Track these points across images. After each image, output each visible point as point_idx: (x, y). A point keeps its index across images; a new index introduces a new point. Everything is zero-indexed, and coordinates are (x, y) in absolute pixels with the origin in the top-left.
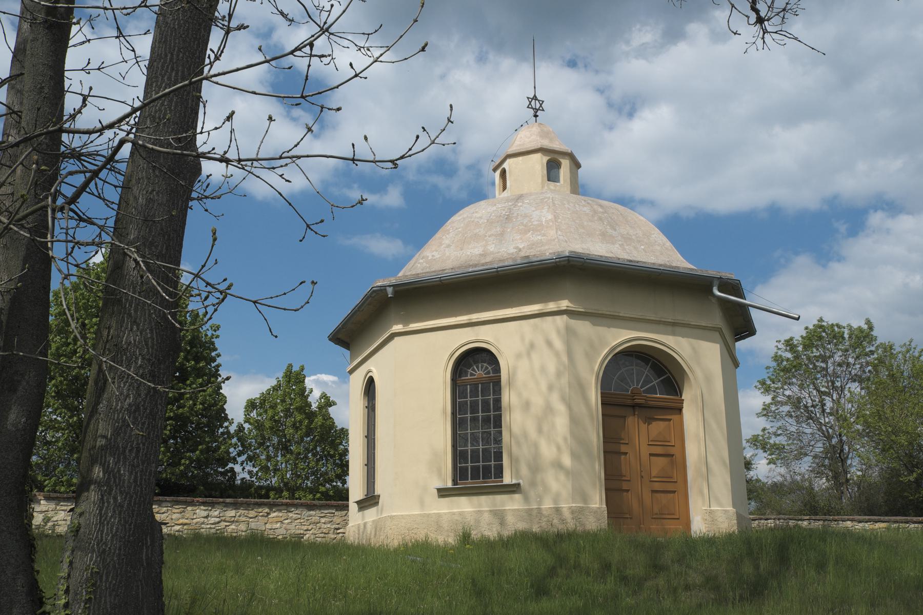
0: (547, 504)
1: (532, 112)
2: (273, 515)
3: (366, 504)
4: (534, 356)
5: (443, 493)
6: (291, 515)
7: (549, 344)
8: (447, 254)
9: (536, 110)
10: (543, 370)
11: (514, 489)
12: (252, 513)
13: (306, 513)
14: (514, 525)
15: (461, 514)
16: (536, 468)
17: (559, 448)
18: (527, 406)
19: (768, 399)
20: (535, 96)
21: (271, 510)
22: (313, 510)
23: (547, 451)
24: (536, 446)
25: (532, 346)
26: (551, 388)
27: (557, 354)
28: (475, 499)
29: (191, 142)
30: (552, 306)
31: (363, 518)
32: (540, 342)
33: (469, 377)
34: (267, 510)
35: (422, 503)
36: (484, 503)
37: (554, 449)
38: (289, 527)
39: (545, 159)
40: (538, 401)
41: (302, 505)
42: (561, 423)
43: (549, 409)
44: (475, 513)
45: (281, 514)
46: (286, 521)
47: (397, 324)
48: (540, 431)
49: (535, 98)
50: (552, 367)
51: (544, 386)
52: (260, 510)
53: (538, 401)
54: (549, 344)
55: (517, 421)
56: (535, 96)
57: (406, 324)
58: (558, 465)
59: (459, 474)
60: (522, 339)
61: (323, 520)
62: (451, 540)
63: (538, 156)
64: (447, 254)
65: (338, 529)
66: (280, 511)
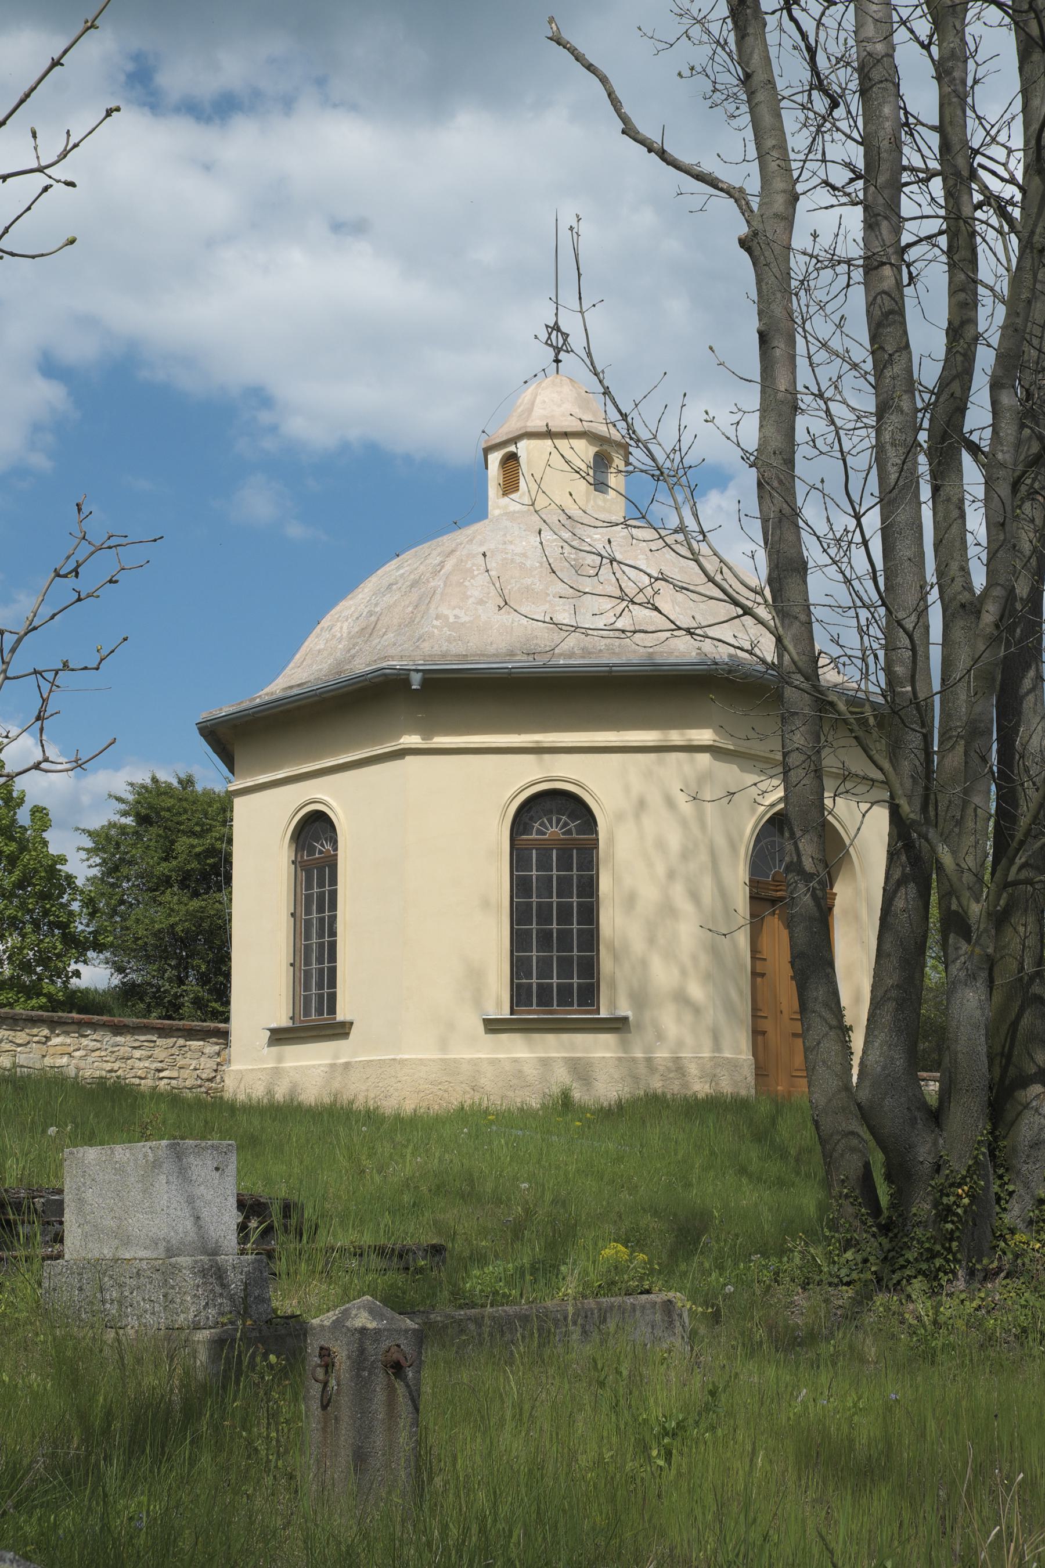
0: (662, 1054)
1: (551, 353)
2: (56, 1040)
3: (303, 1035)
4: (647, 822)
5: (493, 1026)
6: (85, 1042)
7: (670, 803)
8: (484, 617)
9: (558, 350)
10: (661, 845)
11: (618, 1025)
12: (21, 1037)
13: (109, 1039)
14: (608, 1088)
15: (516, 1060)
16: (641, 999)
17: (684, 973)
18: (631, 900)
19: (44, 835)
20: (556, 323)
21: (52, 1031)
22: (121, 1034)
23: (662, 975)
24: (644, 963)
25: (641, 805)
26: (671, 875)
27: (684, 823)
28: (565, 1037)
29: (807, 600)
30: (676, 737)
31: (280, 1059)
32: (655, 799)
33: (534, 836)
34: (46, 1032)
35: (443, 1044)
36: (555, 1047)
37: (676, 972)
38: (82, 1064)
39: (592, 450)
40: (649, 894)
41: (104, 1026)
42: (687, 932)
43: (668, 910)
44: (531, 1065)
45: (68, 1041)
46: (77, 1054)
47: (410, 732)
48: (652, 941)
49: (556, 328)
50: (675, 840)
51: (661, 870)
52: (35, 1031)
53: (649, 894)
54: (670, 803)
55: (623, 918)
56: (556, 323)
57: (427, 735)
58: (681, 998)
59: (519, 996)
60: (627, 789)
61: (137, 1054)
62: (535, 1103)
63: (580, 444)
64: (484, 617)
65: (160, 1071)
66: (67, 1033)
